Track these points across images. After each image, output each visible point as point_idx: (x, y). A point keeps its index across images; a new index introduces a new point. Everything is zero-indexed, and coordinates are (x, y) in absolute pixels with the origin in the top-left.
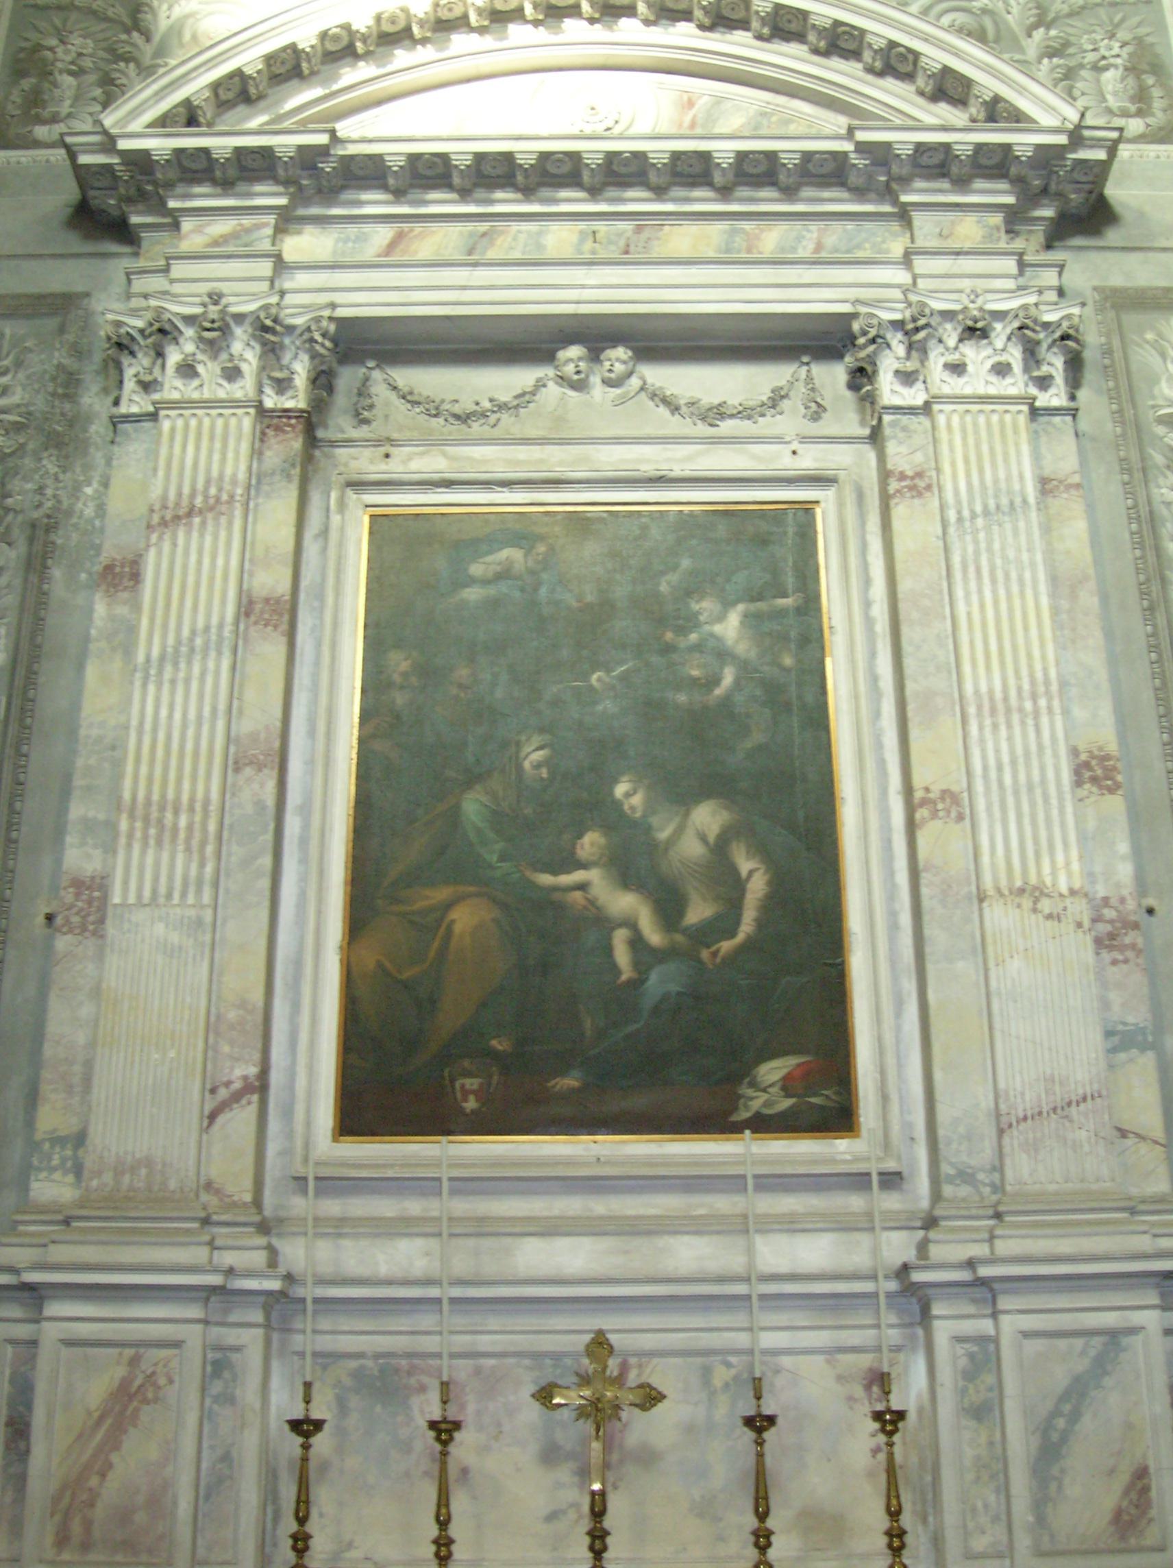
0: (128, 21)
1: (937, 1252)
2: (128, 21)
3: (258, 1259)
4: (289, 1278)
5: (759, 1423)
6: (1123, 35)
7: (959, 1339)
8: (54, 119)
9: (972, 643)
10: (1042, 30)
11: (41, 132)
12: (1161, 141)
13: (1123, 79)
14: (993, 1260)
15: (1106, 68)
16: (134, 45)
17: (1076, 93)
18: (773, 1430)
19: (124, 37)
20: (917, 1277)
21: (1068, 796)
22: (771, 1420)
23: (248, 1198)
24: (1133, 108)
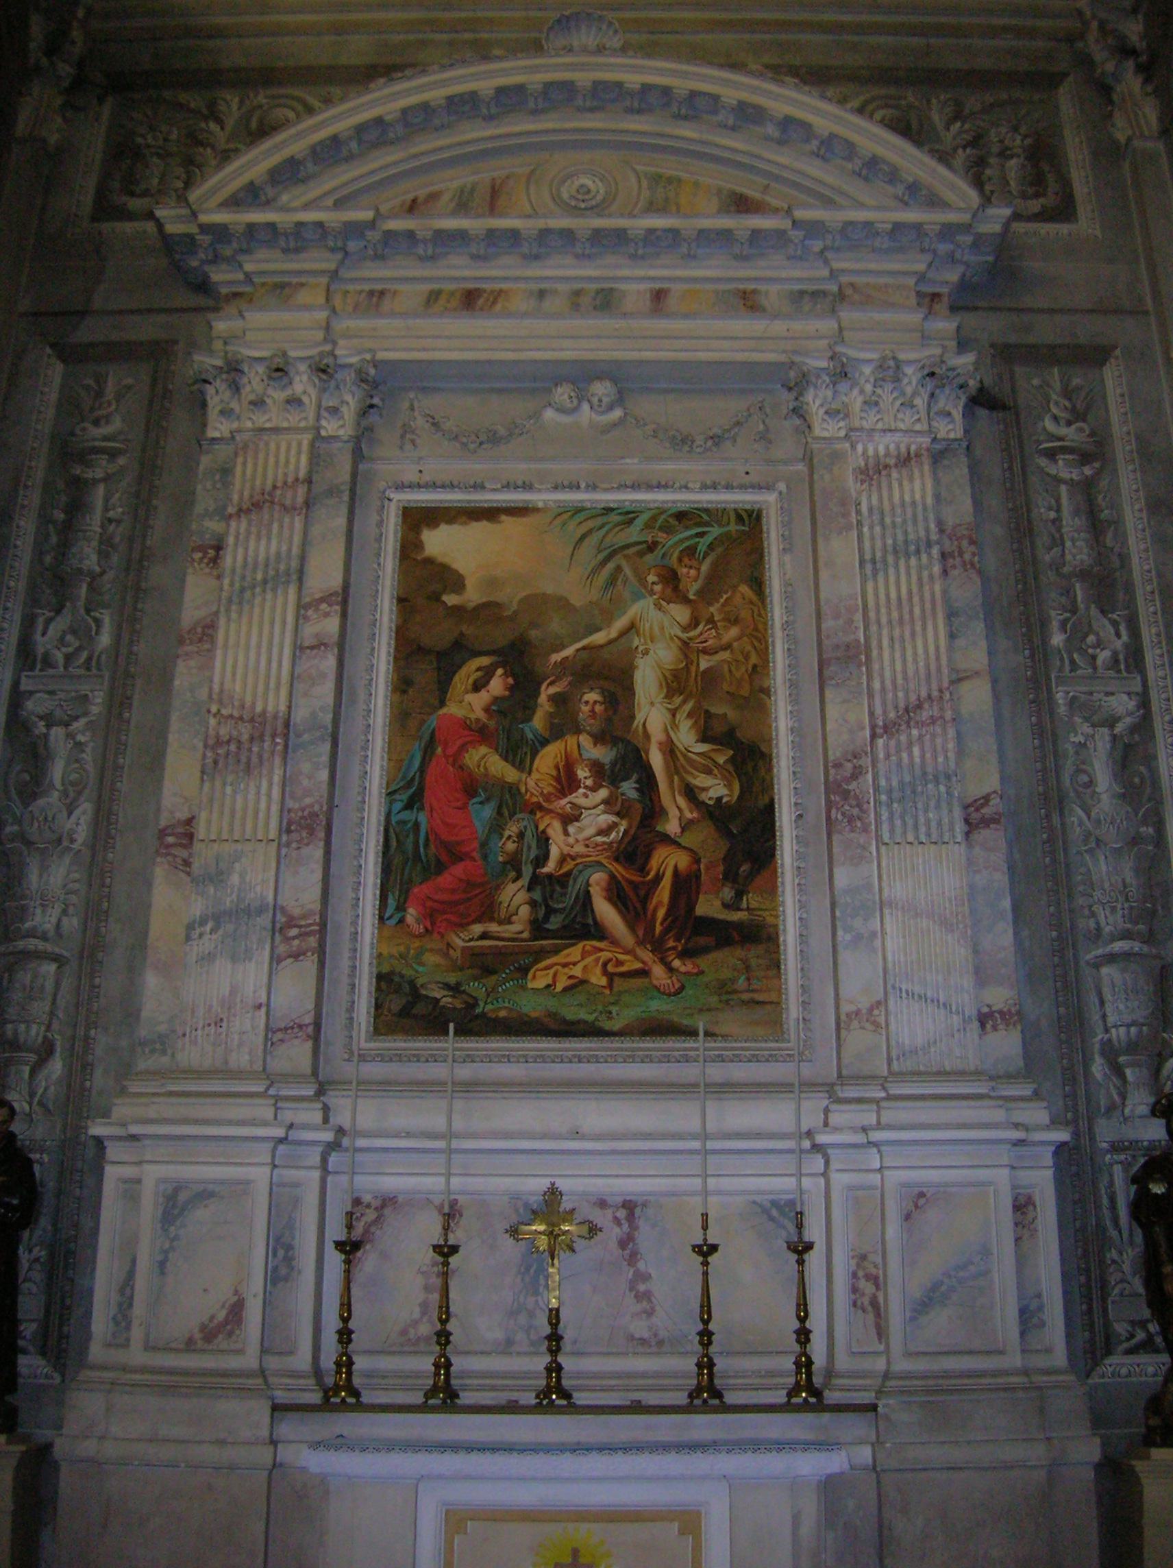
0: (205, 111)
1: (834, 1119)
2: (205, 111)
3: (317, 1117)
4: (341, 1131)
5: (706, 1251)
6: (1023, 130)
7: (240, 1352)
8: (146, 193)
9: (449, 147)
10: (958, 124)
11: (135, 204)
12: (1051, 219)
13: (1023, 166)
14: (879, 1126)
15: (1012, 157)
16: (211, 133)
17: (984, 178)
18: (716, 1255)
19: (203, 125)
20: (822, 1139)
21: (300, 127)
22: (714, 1248)
23: (309, 1071)
24: (1031, 191)
